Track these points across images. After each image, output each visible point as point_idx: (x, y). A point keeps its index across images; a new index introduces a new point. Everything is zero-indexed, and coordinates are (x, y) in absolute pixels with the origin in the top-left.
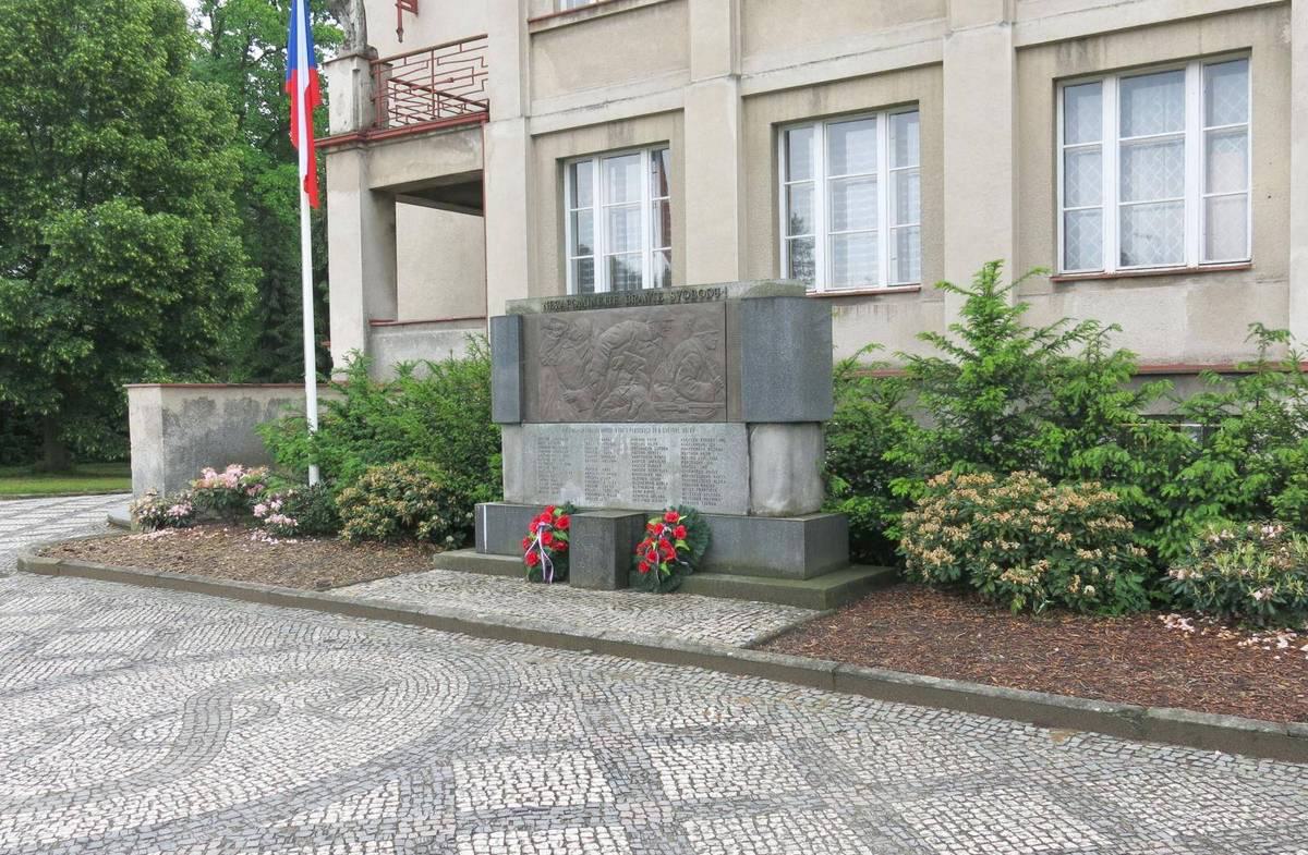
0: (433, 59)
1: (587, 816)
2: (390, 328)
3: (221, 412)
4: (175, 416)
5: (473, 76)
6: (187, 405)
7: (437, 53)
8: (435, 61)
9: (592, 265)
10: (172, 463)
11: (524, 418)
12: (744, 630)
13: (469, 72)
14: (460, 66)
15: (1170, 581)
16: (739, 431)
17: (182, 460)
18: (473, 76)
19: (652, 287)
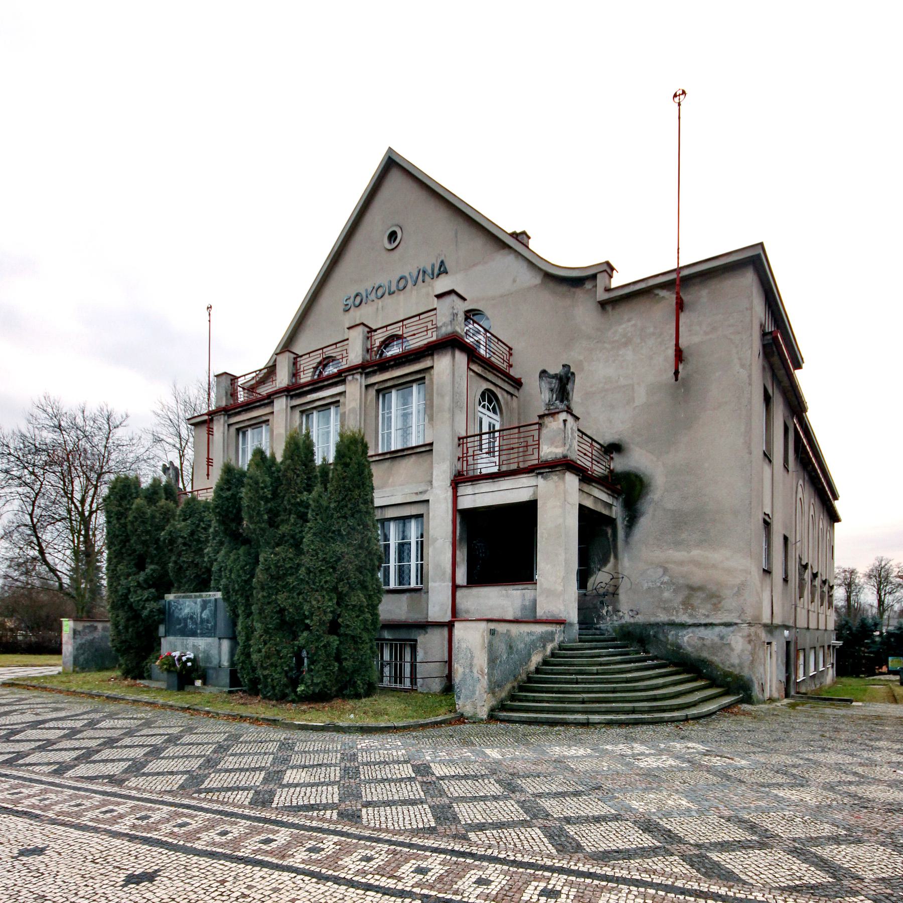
0: (499, 465)
1: (410, 779)
2: (669, 729)
3: (100, 630)
4: (79, 632)
5: (427, 331)
6: (85, 628)
7: (405, 323)
8: (497, 464)
9: (410, 544)
10: (77, 649)
11: (165, 636)
12: (101, 813)
13: (425, 329)
14: (419, 327)
15: (376, 545)
16: (216, 639)
17: (81, 648)
18: (427, 331)
19: (378, 503)
